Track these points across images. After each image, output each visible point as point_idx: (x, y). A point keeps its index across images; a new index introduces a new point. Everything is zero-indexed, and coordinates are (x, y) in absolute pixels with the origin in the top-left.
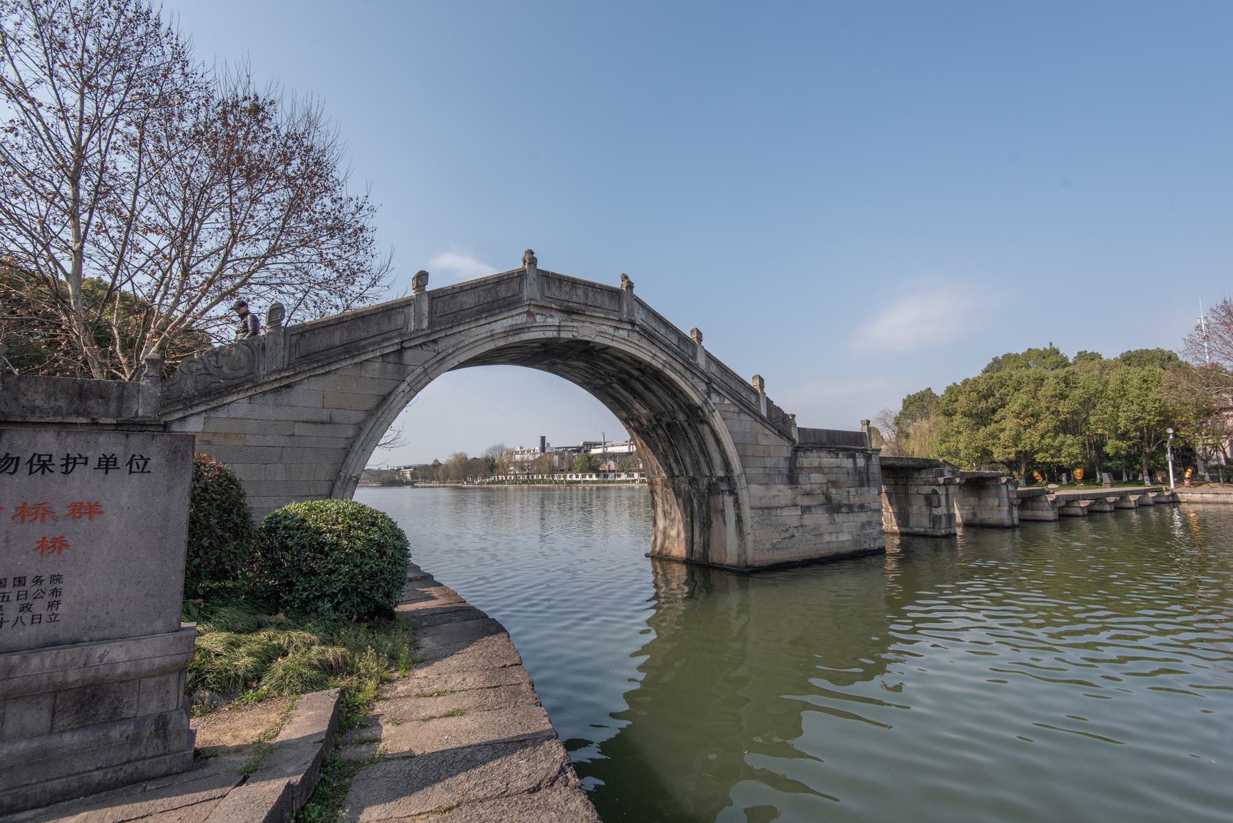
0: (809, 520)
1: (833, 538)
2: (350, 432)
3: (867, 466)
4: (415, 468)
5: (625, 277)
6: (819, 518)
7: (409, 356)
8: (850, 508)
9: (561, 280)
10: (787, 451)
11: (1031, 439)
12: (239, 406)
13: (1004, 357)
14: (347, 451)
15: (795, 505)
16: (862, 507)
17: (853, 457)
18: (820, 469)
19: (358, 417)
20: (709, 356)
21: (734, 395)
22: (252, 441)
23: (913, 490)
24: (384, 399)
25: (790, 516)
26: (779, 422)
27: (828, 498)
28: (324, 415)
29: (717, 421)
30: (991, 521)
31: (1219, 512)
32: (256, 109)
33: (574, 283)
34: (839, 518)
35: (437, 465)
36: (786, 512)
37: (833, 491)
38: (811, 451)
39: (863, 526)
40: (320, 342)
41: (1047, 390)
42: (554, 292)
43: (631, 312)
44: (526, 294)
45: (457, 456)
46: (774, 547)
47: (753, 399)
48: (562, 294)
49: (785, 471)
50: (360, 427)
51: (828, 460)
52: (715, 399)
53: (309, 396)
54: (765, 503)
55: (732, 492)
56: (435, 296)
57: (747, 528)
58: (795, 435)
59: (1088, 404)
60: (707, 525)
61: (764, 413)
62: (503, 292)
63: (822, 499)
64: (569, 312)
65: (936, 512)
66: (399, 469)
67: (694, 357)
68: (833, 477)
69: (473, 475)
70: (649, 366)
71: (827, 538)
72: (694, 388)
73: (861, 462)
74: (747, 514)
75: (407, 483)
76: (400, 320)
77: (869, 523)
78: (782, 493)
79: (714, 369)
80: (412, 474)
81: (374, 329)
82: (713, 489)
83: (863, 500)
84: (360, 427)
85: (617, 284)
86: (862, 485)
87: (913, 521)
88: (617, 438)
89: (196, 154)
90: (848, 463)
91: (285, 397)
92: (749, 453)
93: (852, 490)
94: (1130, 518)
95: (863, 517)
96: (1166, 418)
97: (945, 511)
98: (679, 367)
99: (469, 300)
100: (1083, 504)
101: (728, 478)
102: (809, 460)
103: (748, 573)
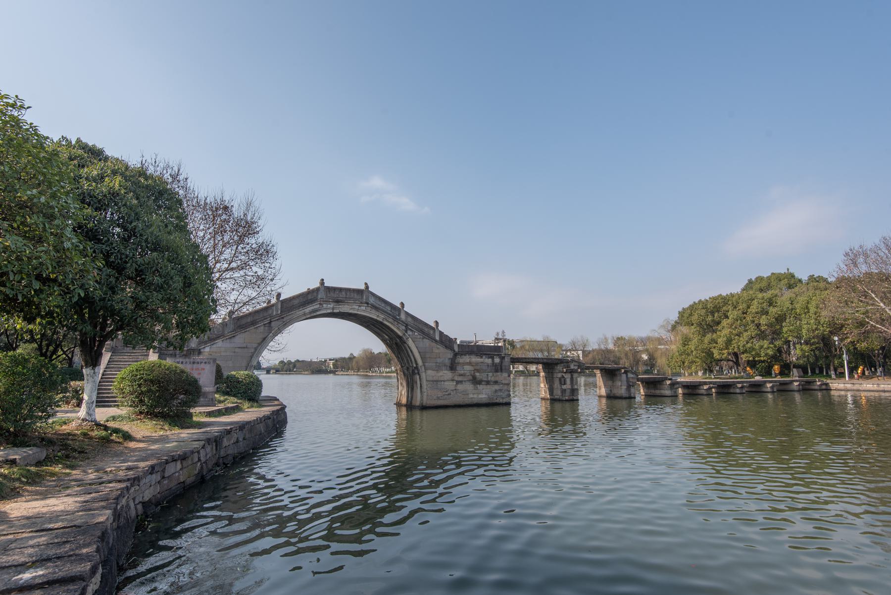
0: (460, 387)
1: (475, 396)
2: (253, 350)
3: (501, 362)
4: (336, 361)
5: (366, 284)
6: (469, 387)
7: (273, 324)
8: (488, 383)
9: (334, 289)
10: (450, 355)
11: (740, 343)
12: (219, 343)
13: (757, 278)
14: (251, 357)
15: (453, 380)
16: (496, 382)
17: (493, 358)
18: (470, 364)
19: (255, 345)
20: (407, 313)
21: (422, 332)
22: (223, 354)
23: (555, 375)
24: (264, 339)
25: (450, 385)
26: (446, 342)
27: (474, 378)
28: (244, 345)
29: (410, 343)
30: (618, 395)
31: (880, 398)
32: (226, 208)
33: (341, 290)
34: (480, 387)
35: (352, 358)
36: (446, 383)
37: (477, 374)
38: (465, 355)
39: (496, 391)
40: (244, 322)
41: (754, 308)
42: (332, 294)
43: (367, 298)
44: (319, 296)
45: (365, 351)
46: (438, 398)
47: (432, 332)
48: (335, 295)
49: (449, 365)
50: (256, 349)
51: (475, 359)
52: (410, 333)
53: (241, 339)
54: (435, 379)
55: (419, 374)
56: (283, 302)
57: (424, 390)
58: (456, 349)
59: (780, 319)
60: (412, 389)
61: (437, 338)
62: (310, 297)
63: (471, 378)
64: (338, 302)
65: (564, 387)
66: (326, 361)
67: (399, 315)
68: (478, 368)
69: (287, 368)
70: (376, 321)
71: (471, 396)
72: (398, 328)
73: (497, 360)
74: (425, 383)
75: (331, 372)
76: (270, 312)
77: (500, 390)
78: (447, 374)
79: (410, 319)
80: (334, 365)
81: (261, 315)
82: (414, 373)
83: (497, 379)
84: (256, 349)
85: (363, 287)
86: (497, 371)
87: (555, 392)
88: (378, 346)
89: (202, 227)
90: (489, 361)
91: (233, 340)
92: (427, 356)
93: (490, 374)
94: (767, 397)
95: (497, 387)
96: (837, 328)
97: (569, 387)
98: (390, 320)
99: (296, 302)
100: (706, 387)
101: (417, 368)
102: (461, 360)
103: (424, 408)
